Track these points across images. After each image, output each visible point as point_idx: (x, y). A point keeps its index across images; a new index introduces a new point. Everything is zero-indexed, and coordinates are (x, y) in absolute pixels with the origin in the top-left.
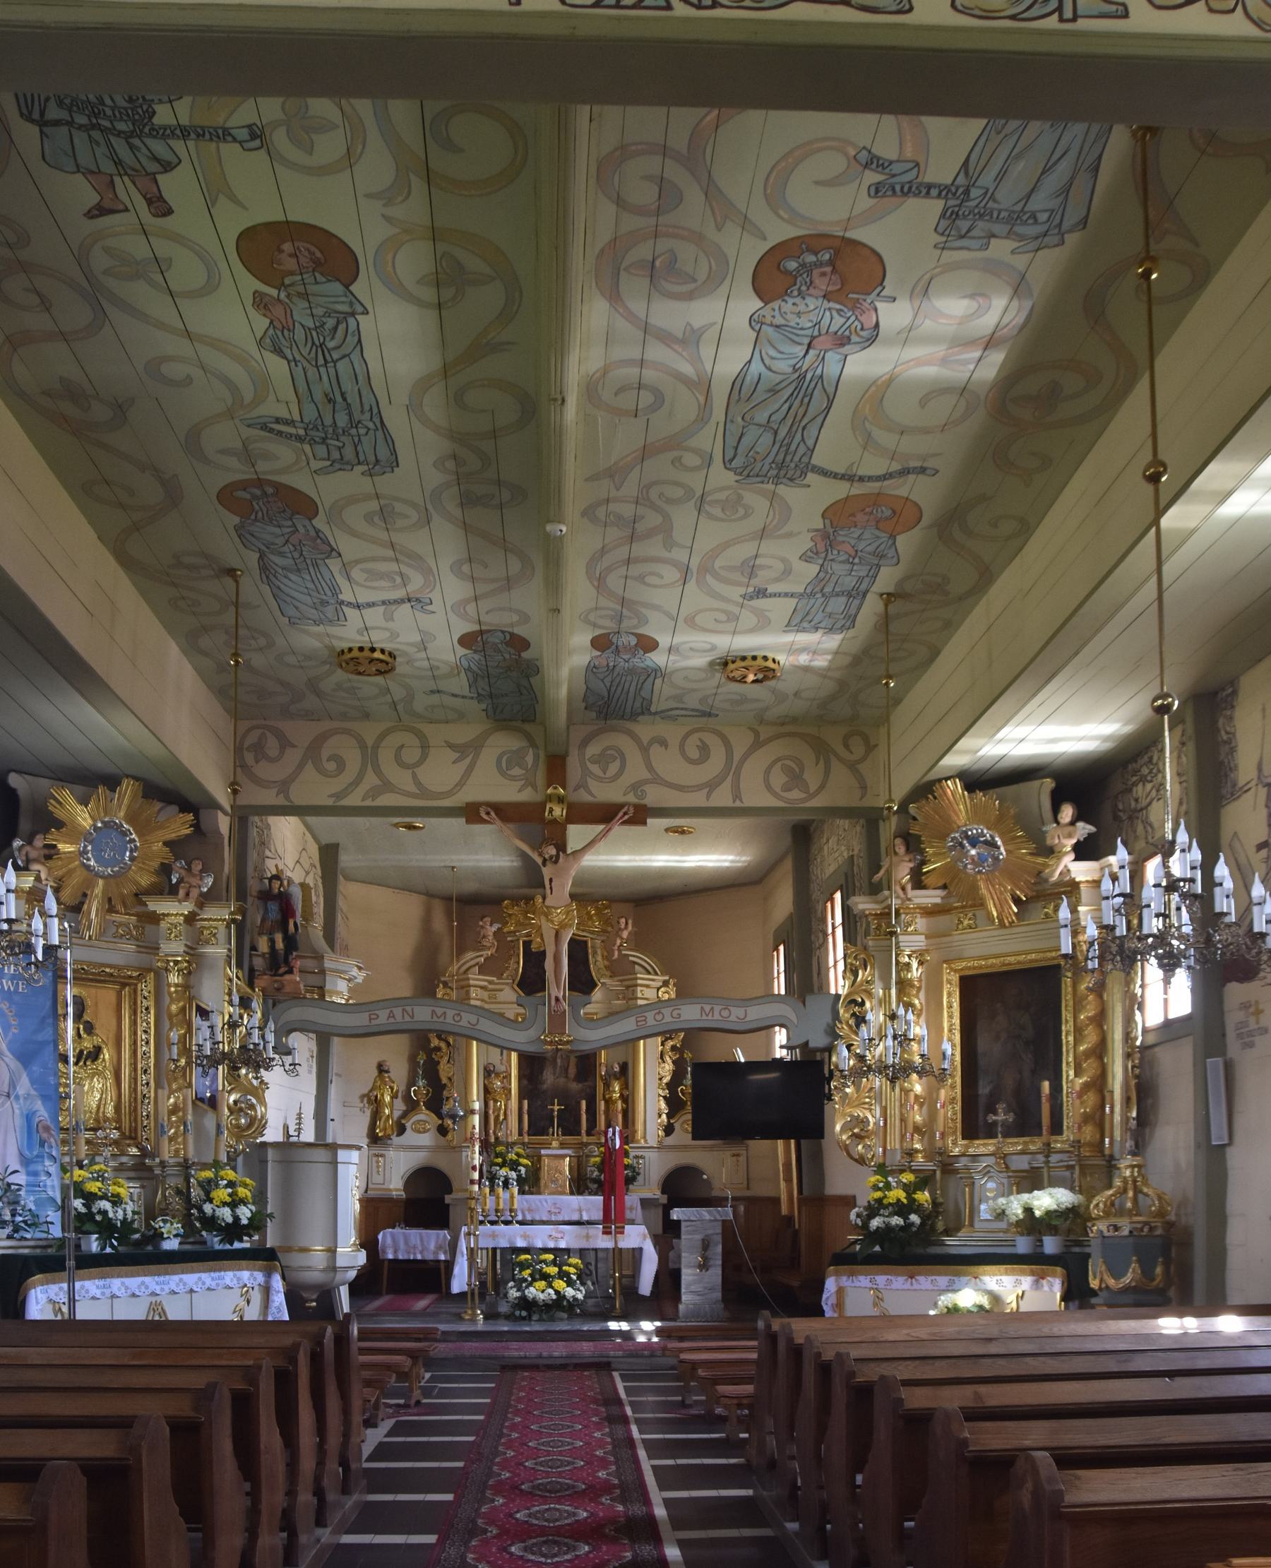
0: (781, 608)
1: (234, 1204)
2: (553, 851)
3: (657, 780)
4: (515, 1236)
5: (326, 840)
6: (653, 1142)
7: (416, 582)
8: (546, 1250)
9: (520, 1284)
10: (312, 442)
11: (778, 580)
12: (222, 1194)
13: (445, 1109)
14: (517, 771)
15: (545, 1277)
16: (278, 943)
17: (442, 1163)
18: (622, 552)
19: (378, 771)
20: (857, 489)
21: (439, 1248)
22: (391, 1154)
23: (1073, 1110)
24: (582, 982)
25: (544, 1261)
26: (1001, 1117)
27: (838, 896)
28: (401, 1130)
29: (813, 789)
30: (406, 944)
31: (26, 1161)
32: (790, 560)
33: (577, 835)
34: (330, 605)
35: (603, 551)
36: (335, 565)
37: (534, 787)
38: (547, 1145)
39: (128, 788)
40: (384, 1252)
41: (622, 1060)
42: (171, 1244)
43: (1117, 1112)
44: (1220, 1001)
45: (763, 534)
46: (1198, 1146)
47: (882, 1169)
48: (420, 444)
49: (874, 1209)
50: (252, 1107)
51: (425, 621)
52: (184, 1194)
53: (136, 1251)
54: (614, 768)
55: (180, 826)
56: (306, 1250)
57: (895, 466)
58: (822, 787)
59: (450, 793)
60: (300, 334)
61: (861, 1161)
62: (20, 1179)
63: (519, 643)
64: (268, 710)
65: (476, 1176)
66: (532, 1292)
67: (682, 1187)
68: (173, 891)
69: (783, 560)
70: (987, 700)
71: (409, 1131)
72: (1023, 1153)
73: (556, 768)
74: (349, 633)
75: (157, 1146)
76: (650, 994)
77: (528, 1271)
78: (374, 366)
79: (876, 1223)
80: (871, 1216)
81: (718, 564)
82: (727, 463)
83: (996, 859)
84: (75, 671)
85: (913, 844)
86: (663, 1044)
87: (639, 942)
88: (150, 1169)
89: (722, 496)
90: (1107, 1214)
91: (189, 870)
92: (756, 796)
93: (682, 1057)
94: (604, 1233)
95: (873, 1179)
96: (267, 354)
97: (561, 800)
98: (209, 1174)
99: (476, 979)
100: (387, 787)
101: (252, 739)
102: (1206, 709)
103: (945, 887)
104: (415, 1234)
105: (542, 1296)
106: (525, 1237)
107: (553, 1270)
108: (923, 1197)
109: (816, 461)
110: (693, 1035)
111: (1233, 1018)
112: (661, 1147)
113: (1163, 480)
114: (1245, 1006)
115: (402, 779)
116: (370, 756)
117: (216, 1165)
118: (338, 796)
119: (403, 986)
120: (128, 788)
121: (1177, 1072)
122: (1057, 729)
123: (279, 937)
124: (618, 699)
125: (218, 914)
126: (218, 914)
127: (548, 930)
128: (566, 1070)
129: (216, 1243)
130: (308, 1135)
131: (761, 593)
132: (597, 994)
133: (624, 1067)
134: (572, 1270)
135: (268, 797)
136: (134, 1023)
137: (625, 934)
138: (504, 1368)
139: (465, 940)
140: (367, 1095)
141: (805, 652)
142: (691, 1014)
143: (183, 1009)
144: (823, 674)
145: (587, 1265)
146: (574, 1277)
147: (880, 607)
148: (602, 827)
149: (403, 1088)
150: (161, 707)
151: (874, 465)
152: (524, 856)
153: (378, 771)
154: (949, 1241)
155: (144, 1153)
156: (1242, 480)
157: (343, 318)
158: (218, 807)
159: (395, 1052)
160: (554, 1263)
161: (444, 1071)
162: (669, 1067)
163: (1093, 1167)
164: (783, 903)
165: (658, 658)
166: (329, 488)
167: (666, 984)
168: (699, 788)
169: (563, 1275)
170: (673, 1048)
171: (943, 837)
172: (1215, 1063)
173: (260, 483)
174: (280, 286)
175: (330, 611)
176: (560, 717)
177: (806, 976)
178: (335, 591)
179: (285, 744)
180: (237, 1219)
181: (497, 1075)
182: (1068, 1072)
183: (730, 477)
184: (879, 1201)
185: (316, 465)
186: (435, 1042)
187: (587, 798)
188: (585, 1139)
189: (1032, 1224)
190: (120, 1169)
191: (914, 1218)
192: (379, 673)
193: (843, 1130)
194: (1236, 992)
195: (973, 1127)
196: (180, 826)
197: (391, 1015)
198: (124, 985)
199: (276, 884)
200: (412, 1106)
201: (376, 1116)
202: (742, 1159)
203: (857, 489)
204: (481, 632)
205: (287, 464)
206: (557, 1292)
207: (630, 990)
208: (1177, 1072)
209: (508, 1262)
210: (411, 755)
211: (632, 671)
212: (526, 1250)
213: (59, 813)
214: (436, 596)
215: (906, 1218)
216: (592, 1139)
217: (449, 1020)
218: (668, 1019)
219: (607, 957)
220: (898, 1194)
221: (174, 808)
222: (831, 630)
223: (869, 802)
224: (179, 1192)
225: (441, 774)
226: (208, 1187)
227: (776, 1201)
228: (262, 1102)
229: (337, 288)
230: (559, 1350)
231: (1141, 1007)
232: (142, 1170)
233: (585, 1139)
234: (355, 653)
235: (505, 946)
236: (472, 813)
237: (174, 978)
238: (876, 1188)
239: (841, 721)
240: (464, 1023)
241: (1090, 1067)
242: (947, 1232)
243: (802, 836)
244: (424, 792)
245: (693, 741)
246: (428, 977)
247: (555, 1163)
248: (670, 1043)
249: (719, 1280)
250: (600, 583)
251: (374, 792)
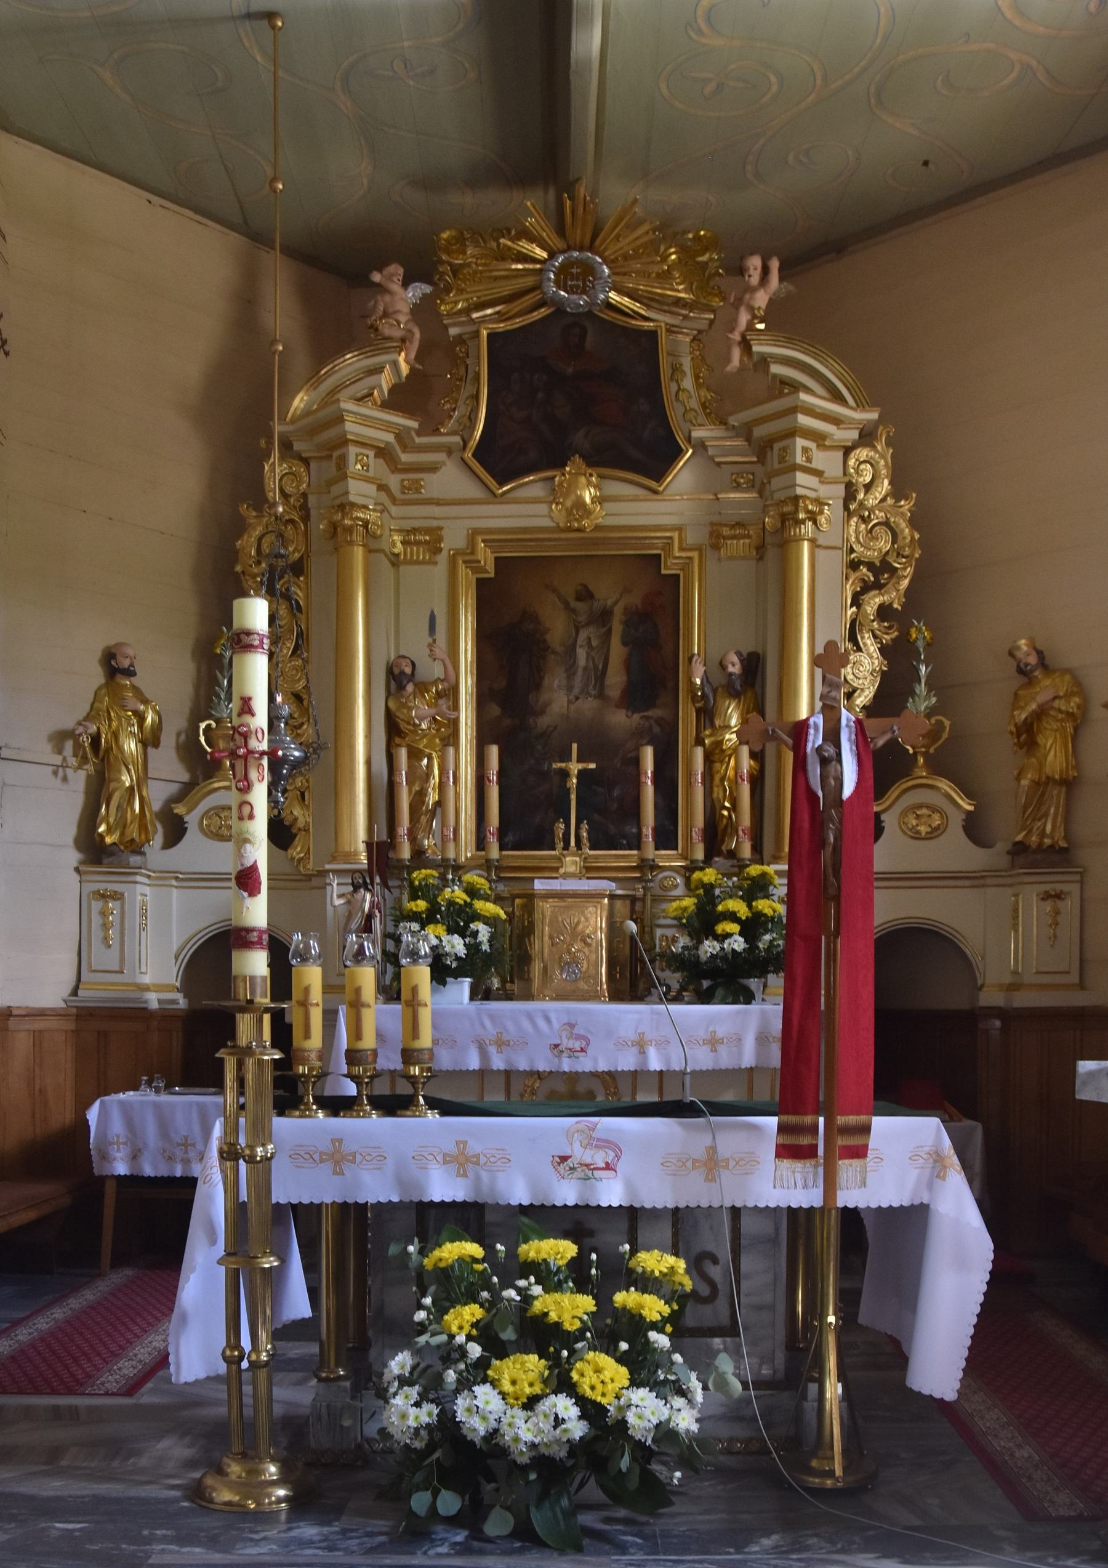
8: (544, 1218)
15: (542, 1336)
22: (142, 892)
25: (541, 1271)
28: (175, 831)
38: (551, 870)
40: (105, 1157)
41: (748, 648)
66: (483, 1408)
71: (193, 836)
77: (471, 1313)
86: (856, 601)
93: (904, 635)
94: (784, 1152)
105: (524, 1431)
106: (461, 1161)
107: (570, 1308)
128: (601, 676)
132: (683, 476)
133: (753, 664)
134: (654, 1307)
139: (339, 322)
146: (661, 1340)
160: (578, 1275)
169: (617, 1332)
170: (884, 612)
181: (422, 688)
201: (98, 790)
202: (1069, 907)
206: (590, 1410)
212: (469, 1218)
235: (439, 352)
248: (873, 602)
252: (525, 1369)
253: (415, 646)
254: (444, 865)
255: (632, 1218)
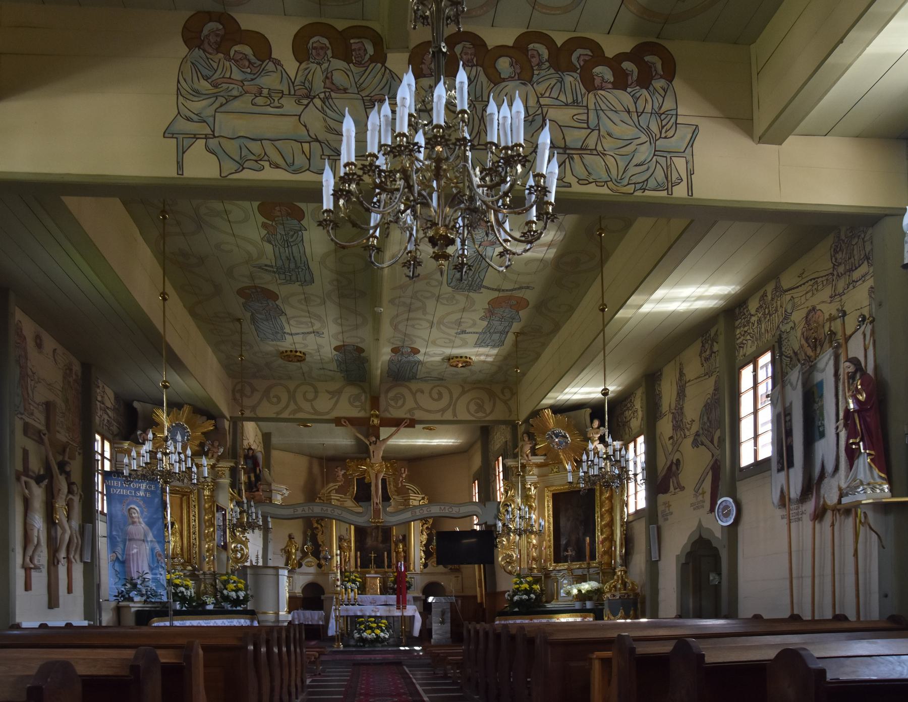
0: (472, 338)
1: (237, 590)
2: (374, 439)
3: (420, 408)
4: (356, 610)
5: (265, 431)
6: (418, 571)
7: (317, 326)
8: (370, 617)
9: (359, 631)
10: (279, 273)
11: (470, 327)
12: (231, 586)
13: (322, 555)
14: (357, 404)
16: (252, 476)
17: (320, 581)
18: (405, 316)
19: (296, 403)
20: (501, 294)
21: (320, 619)
23: (600, 549)
24: (386, 498)
25: (371, 622)
26: (570, 553)
27: (501, 458)
28: (300, 565)
29: (488, 412)
30: (301, 479)
31: (151, 569)
32: (475, 319)
33: (384, 432)
34: (280, 334)
35: (397, 315)
36: (283, 319)
37: (365, 410)
39: (186, 409)
42: (210, 607)
43: (619, 551)
44: (656, 501)
45: (464, 310)
46: (647, 561)
47: (519, 576)
48: (323, 277)
49: (516, 592)
50: (242, 549)
51: (319, 340)
52: (214, 586)
53: (196, 609)
54: (400, 402)
55: (209, 426)
56: (265, 613)
57: (517, 286)
58: (491, 412)
59: (328, 413)
60: (279, 237)
61: (510, 573)
62: (149, 576)
63: (360, 350)
64: (244, 376)
65: (339, 583)
66: (365, 635)
67: (429, 589)
68: (206, 454)
69: (473, 320)
70: (558, 378)
71: (304, 566)
72: (579, 568)
73: (375, 402)
74: (287, 344)
75: (201, 564)
76: (416, 503)
78: (308, 250)
79: (516, 598)
80: (514, 596)
81: (445, 321)
82: (448, 284)
83: (567, 443)
84: (175, 362)
85: (531, 437)
87: (410, 479)
88: (198, 576)
89: (447, 296)
90: (610, 590)
91: (213, 445)
92: (463, 415)
95: (515, 580)
96: (265, 243)
97: (377, 416)
98: (225, 578)
99: (334, 496)
100: (300, 410)
101: (239, 387)
102: (650, 380)
103: (545, 455)
104: (308, 613)
106: (361, 611)
108: (537, 587)
109: (484, 284)
110: (437, 519)
111: (660, 508)
112: (422, 573)
113: (606, 310)
114: (665, 503)
115: (306, 406)
116: (292, 396)
117: (227, 574)
118: (278, 413)
119: (300, 498)
120: (186, 409)
121: (640, 530)
122: (583, 390)
123: (252, 475)
124: (403, 373)
125: (225, 465)
126: (225, 465)
127: (372, 474)
129: (228, 607)
130: (260, 564)
131: (464, 332)
133: (404, 537)
135: (248, 413)
136: (188, 512)
137: (404, 476)
138: (354, 665)
139: (328, 478)
140: (284, 549)
141: (483, 355)
142: (435, 510)
143: (210, 507)
144: (491, 363)
145: (389, 623)
147: (514, 337)
148: (394, 429)
149: (300, 546)
150: (205, 378)
151: (507, 286)
152: (357, 439)
153: (296, 403)
154: (548, 606)
155: (194, 569)
156: (646, 301)
157: (296, 232)
158: (225, 417)
159: (296, 529)
160: (374, 622)
161: (320, 538)
162: (425, 536)
163: (606, 572)
164: (477, 462)
165: (420, 357)
166: (283, 290)
167: (423, 498)
168: (438, 411)
170: (427, 528)
171: (544, 434)
172: (653, 527)
173: (255, 287)
174: (273, 220)
175: (279, 336)
176: (377, 380)
177: (487, 493)
178: (282, 328)
179: (253, 390)
180: (238, 597)
182: (598, 533)
183: (450, 289)
184: (517, 589)
185: (279, 282)
186: (315, 525)
187: (389, 416)
188: (386, 570)
189: (581, 596)
190: (185, 575)
191: (532, 596)
192: (298, 361)
193: (502, 560)
194: (662, 498)
195: (558, 559)
196: (209, 426)
197: (303, 510)
198: (183, 495)
199: (251, 452)
200: (305, 555)
202: (460, 578)
203: (501, 294)
204: (344, 346)
205: (267, 281)
207: (407, 500)
208: (640, 530)
209: (354, 621)
210: (310, 396)
211: (409, 362)
212: (362, 617)
213: (157, 419)
214: (326, 331)
215: (529, 596)
216: (390, 570)
217: (329, 512)
218: (425, 512)
219: (396, 486)
220: (525, 586)
221: (205, 418)
222: (494, 346)
223: (511, 418)
224: (212, 585)
225: (324, 404)
226: (225, 583)
227: (476, 597)
228: (247, 548)
229: (295, 222)
230: (378, 657)
231: (627, 505)
232: (193, 576)
233: (386, 570)
234: (289, 353)
235: (348, 481)
236: (338, 422)
237: (207, 493)
238: (516, 583)
239: (501, 383)
240: (336, 513)
241: (607, 531)
242: (547, 602)
243: (485, 432)
244: (316, 412)
245: (435, 391)
246: (311, 494)
247: (373, 581)
249: (449, 628)
250: (396, 328)
251: (294, 412)
252: (369, 631)
253: (344, 533)
254: (350, 572)
255: (381, 617)
